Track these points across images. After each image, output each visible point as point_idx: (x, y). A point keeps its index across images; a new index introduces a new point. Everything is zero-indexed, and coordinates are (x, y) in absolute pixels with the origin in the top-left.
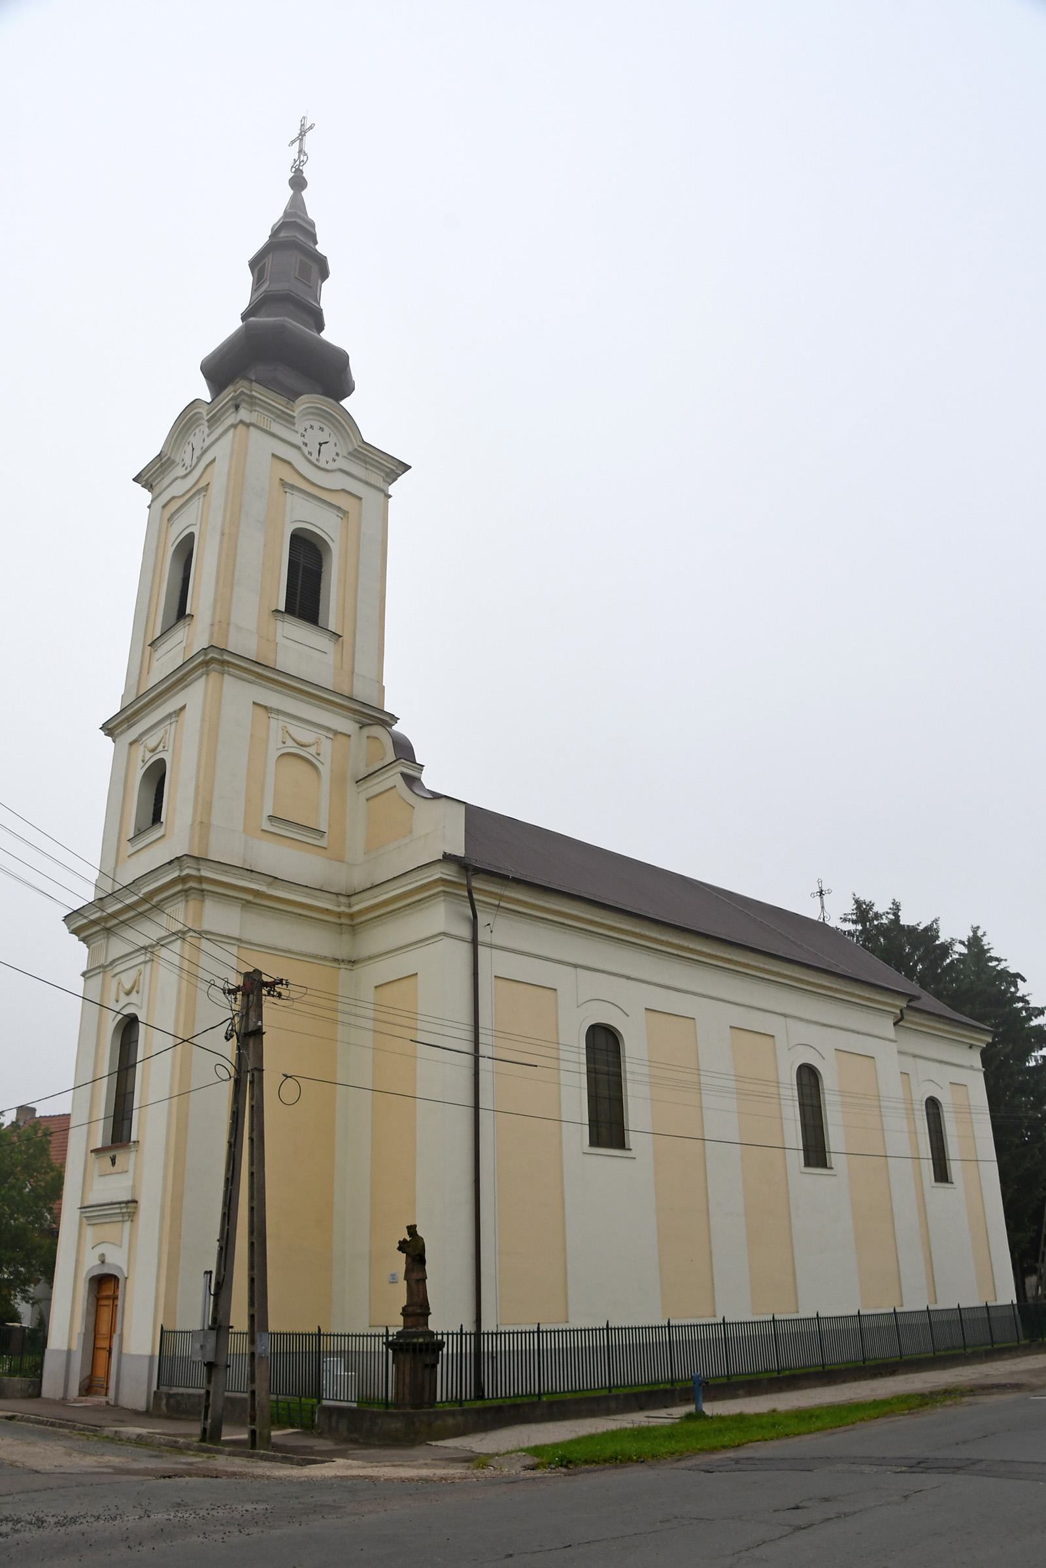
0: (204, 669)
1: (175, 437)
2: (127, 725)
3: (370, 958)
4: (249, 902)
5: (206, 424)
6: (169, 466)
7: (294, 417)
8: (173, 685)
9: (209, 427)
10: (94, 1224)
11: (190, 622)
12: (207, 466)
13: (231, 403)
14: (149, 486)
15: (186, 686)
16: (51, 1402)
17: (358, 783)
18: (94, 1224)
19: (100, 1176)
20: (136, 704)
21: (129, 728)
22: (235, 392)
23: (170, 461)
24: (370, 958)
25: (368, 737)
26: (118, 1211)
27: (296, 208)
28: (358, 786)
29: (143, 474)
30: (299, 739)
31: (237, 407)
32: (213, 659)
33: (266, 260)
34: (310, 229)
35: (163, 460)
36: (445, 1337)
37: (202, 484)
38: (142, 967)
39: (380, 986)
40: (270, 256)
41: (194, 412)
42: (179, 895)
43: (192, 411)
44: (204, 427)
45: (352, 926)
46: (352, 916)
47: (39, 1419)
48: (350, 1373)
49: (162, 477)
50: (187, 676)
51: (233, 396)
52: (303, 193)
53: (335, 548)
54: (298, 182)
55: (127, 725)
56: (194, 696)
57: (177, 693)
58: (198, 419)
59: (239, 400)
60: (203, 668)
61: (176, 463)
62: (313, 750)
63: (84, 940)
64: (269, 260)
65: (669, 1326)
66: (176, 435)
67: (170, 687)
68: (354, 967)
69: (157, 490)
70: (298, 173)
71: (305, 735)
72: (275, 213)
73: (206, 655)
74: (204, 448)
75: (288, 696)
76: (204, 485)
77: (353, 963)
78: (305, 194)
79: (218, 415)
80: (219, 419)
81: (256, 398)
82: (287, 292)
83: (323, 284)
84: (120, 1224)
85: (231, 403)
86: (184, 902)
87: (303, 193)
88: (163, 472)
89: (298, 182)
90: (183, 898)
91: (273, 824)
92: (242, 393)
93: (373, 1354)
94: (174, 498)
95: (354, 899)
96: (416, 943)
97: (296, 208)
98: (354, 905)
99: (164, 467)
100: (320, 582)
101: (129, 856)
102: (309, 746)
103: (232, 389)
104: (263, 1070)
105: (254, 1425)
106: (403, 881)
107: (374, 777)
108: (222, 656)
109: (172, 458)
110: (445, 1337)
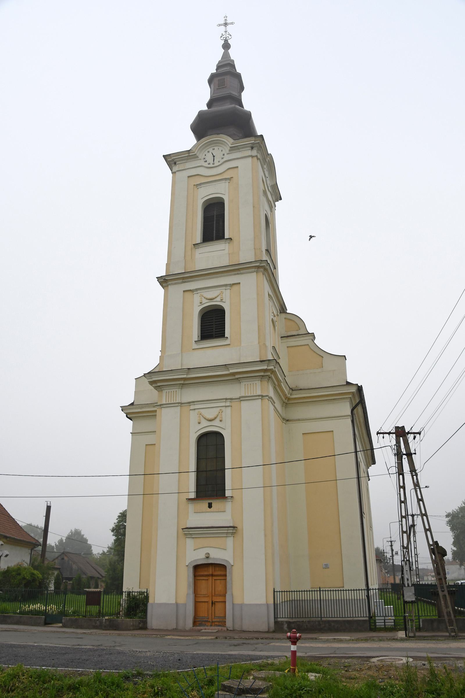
0: (256, 270)
1: (200, 146)
2: (181, 281)
3: (299, 420)
5: (229, 148)
6: (193, 158)
9: (230, 150)
10: (193, 538)
11: (230, 242)
13: (250, 145)
15: (238, 274)
16: (162, 632)
17: (282, 338)
18: (193, 538)
19: (195, 512)
20: (195, 273)
21: (182, 283)
22: (255, 141)
23: (195, 156)
24: (299, 420)
25: (285, 318)
26: (226, 531)
27: (226, 55)
28: (281, 339)
29: (172, 156)
31: (252, 148)
35: (190, 154)
38: (223, 409)
39: (305, 434)
42: (259, 377)
45: (286, 404)
46: (289, 399)
47: (86, 648)
49: (186, 161)
50: (241, 269)
51: (253, 143)
52: (229, 51)
54: (226, 46)
55: (181, 281)
57: (231, 275)
59: (255, 145)
60: (255, 268)
61: (199, 159)
62: (218, 299)
63: (156, 388)
66: (202, 145)
68: (287, 423)
70: (226, 42)
75: (197, 281)
77: (288, 420)
79: (239, 147)
80: (239, 149)
81: (261, 148)
82: (229, 94)
84: (224, 538)
85: (250, 145)
87: (229, 51)
88: (187, 159)
89: (226, 46)
91: (197, 344)
93: (359, 601)
95: (294, 392)
96: (335, 417)
97: (226, 55)
98: (293, 395)
99: (188, 157)
100: (203, 229)
101: (193, 349)
103: (254, 139)
105: (453, 626)
106: (334, 389)
107: (294, 338)
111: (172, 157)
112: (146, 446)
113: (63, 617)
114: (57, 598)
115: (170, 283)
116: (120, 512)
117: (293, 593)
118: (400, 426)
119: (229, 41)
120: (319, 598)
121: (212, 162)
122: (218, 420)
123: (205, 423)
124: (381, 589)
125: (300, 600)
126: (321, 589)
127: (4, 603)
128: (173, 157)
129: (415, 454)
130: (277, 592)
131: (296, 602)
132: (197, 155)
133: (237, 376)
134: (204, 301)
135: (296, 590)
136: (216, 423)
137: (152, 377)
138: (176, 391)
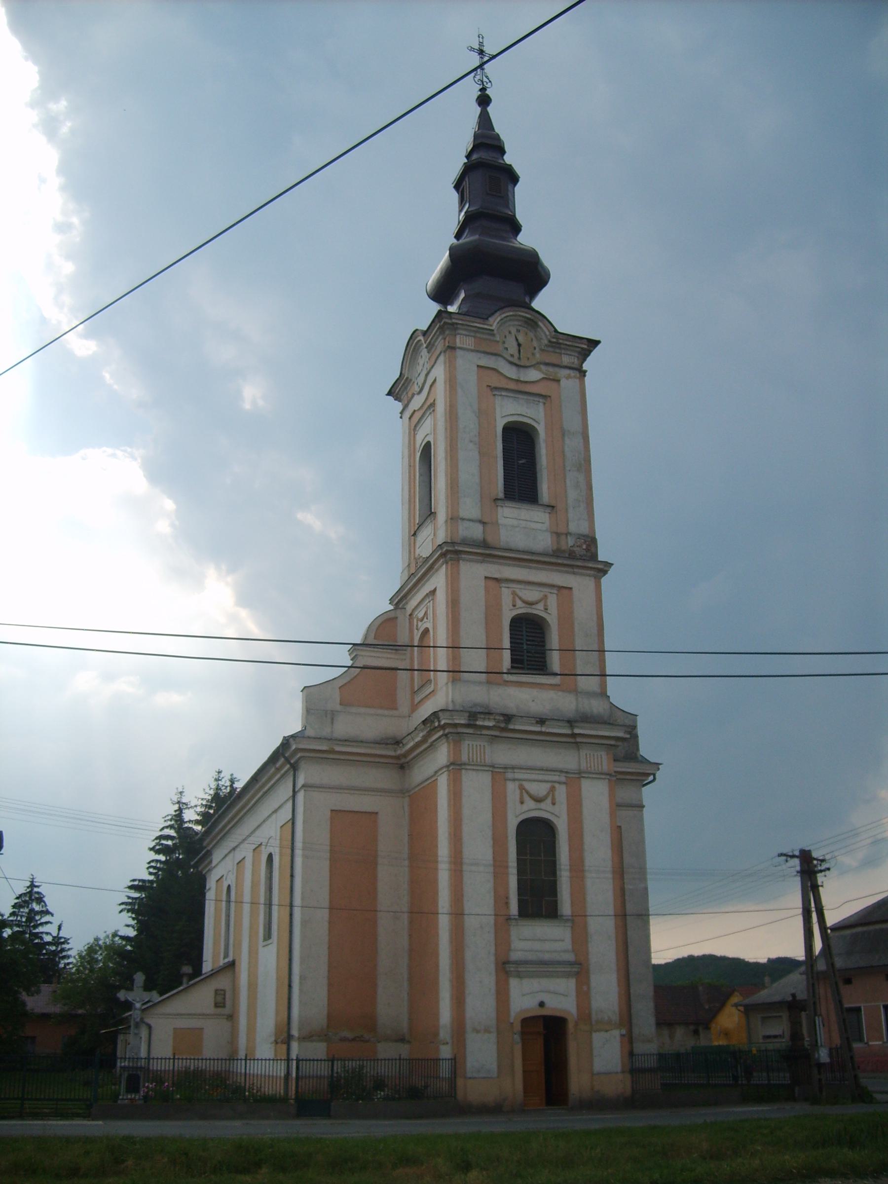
4: (496, 736)
7: (493, 330)
8: (427, 571)
12: (431, 386)
14: (397, 399)
23: (492, 333)
30: (525, 598)
32: (447, 551)
33: (464, 183)
34: (496, 143)
36: (365, 1062)
37: (430, 401)
38: (557, 785)
40: (467, 179)
41: (416, 341)
43: (414, 340)
44: (424, 352)
48: (674, 1074)
53: (541, 429)
54: (484, 100)
56: (439, 580)
58: (420, 343)
62: (541, 606)
64: (466, 183)
65: (400, 1059)
67: (425, 574)
69: (405, 398)
71: (532, 594)
72: (466, 141)
73: (442, 549)
74: (420, 387)
76: (432, 401)
78: (490, 109)
79: (432, 341)
81: (457, 324)
83: (516, 188)
86: (446, 744)
90: (444, 740)
92: (445, 323)
94: (415, 411)
102: (537, 603)
104: (643, 807)
108: (454, 547)
109: (410, 378)
110: (365, 1062)
111: (454, 318)
112: (331, 813)
113: (789, 1082)
114: (446, 1066)
115: (463, 556)
116: (51, 902)
117: (444, 1061)
118: (807, 849)
119: (488, 92)
120: (243, 1071)
121: (516, 355)
122: (549, 801)
123: (530, 804)
124: (148, 1059)
125: (265, 1076)
126: (176, 1057)
127: (322, 1074)
128: (457, 319)
129: (822, 886)
130: (153, 1059)
131: (271, 1079)
132: (495, 332)
133: (579, 740)
134: (519, 603)
135: (268, 1058)
136: (547, 805)
137: (454, 717)
138: (484, 746)
